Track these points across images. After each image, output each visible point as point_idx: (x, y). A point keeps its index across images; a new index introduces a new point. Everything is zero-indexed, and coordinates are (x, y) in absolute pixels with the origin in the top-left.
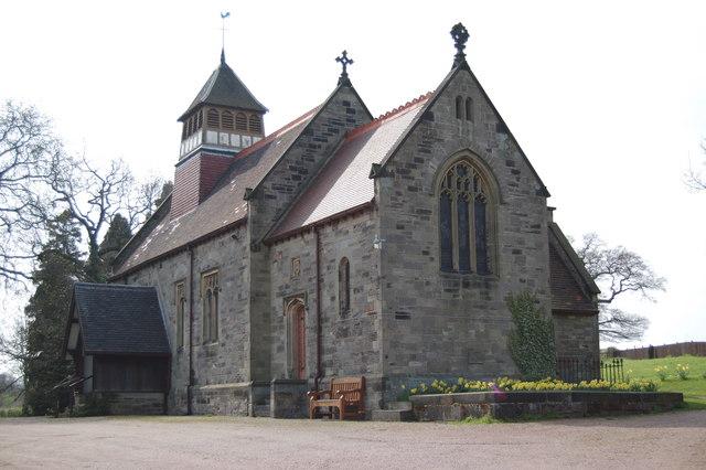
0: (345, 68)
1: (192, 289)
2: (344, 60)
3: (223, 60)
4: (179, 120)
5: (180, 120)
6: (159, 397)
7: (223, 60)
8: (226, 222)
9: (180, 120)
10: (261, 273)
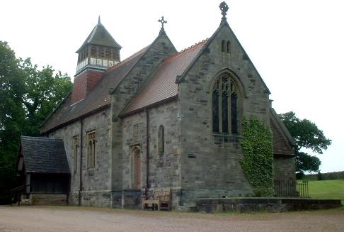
3: (99, 21)
6: (64, 196)
7: (99, 21)
10: (118, 134)
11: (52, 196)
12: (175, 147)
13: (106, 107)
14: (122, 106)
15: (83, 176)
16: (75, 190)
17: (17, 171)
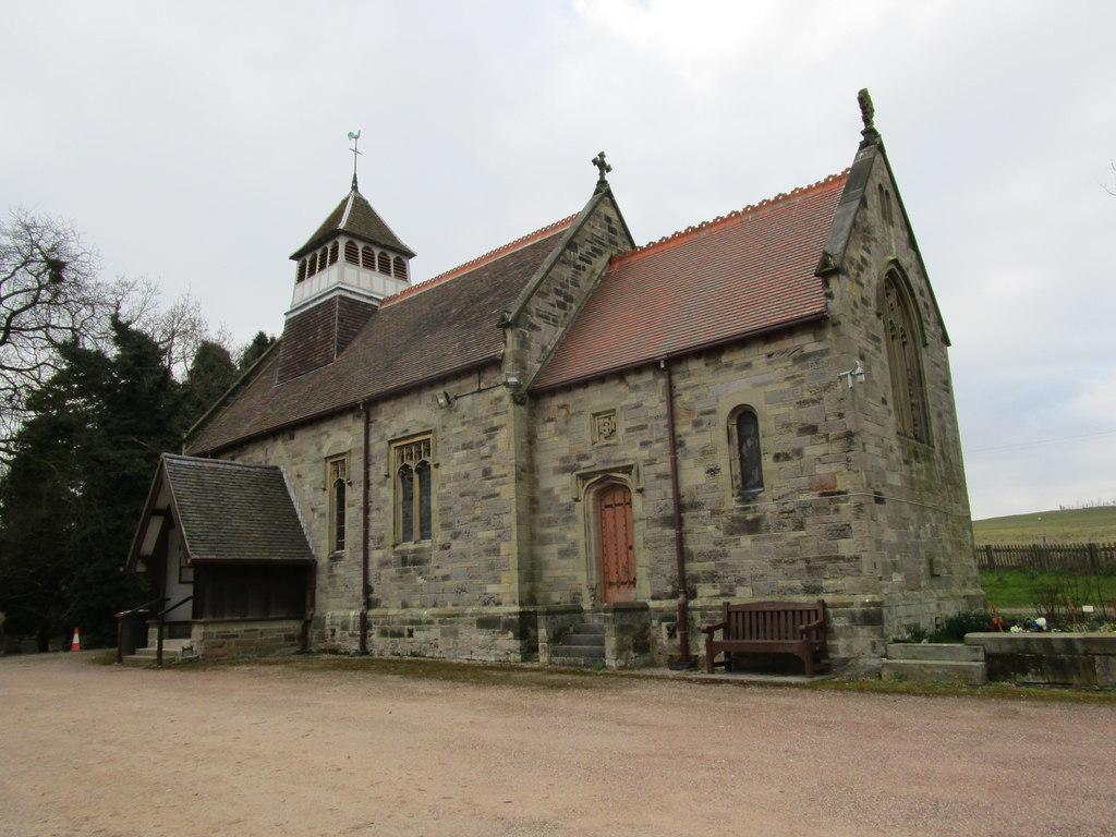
0: (602, 175)
1: (367, 465)
2: (601, 164)
3: (355, 188)
4: (292, 258)
5: (295, 257)
6: (294, 626)
7: (355, 188)
8: (393, 385)
9: (295, 257)
10: (530, 441)
11: (261, 627)
12: (821, 470)
13: (495, 363)
14: (534, 366)
15: (373, 567)
16: (337, 607)
17: (138, 556)
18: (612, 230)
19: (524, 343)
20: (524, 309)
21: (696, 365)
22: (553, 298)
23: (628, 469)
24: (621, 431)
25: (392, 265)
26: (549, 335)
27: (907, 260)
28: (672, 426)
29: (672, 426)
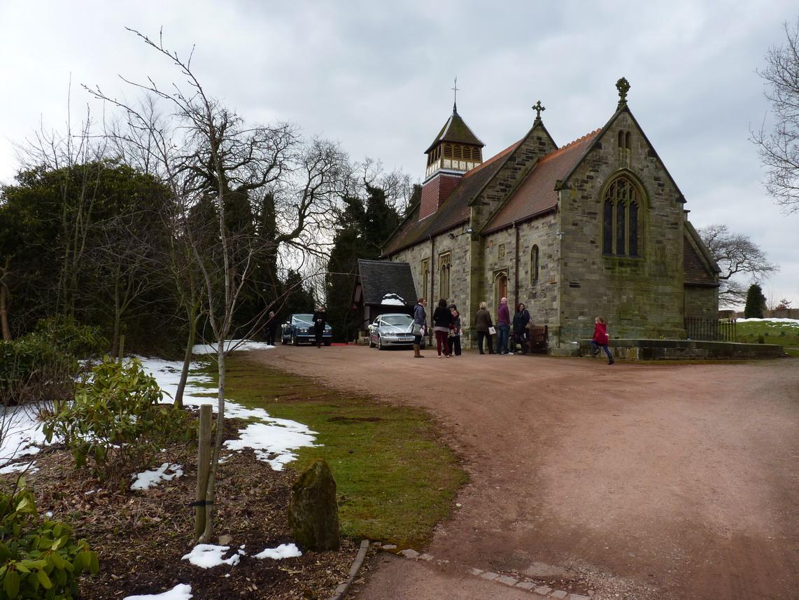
0: (539, 114)
3: (455, 111)
7: (455, 111)
17: (354, 302)
18: (543, 144)
19: (479, 212)
20: (480, 196)
21: (525, 226)
22: (499, 188)
23: (506, 270)
24: (506, 253)
25: (471, 154)
26: (493, 206)
27: (637, 163)
28: (517, 252)
29: (517, 252)
